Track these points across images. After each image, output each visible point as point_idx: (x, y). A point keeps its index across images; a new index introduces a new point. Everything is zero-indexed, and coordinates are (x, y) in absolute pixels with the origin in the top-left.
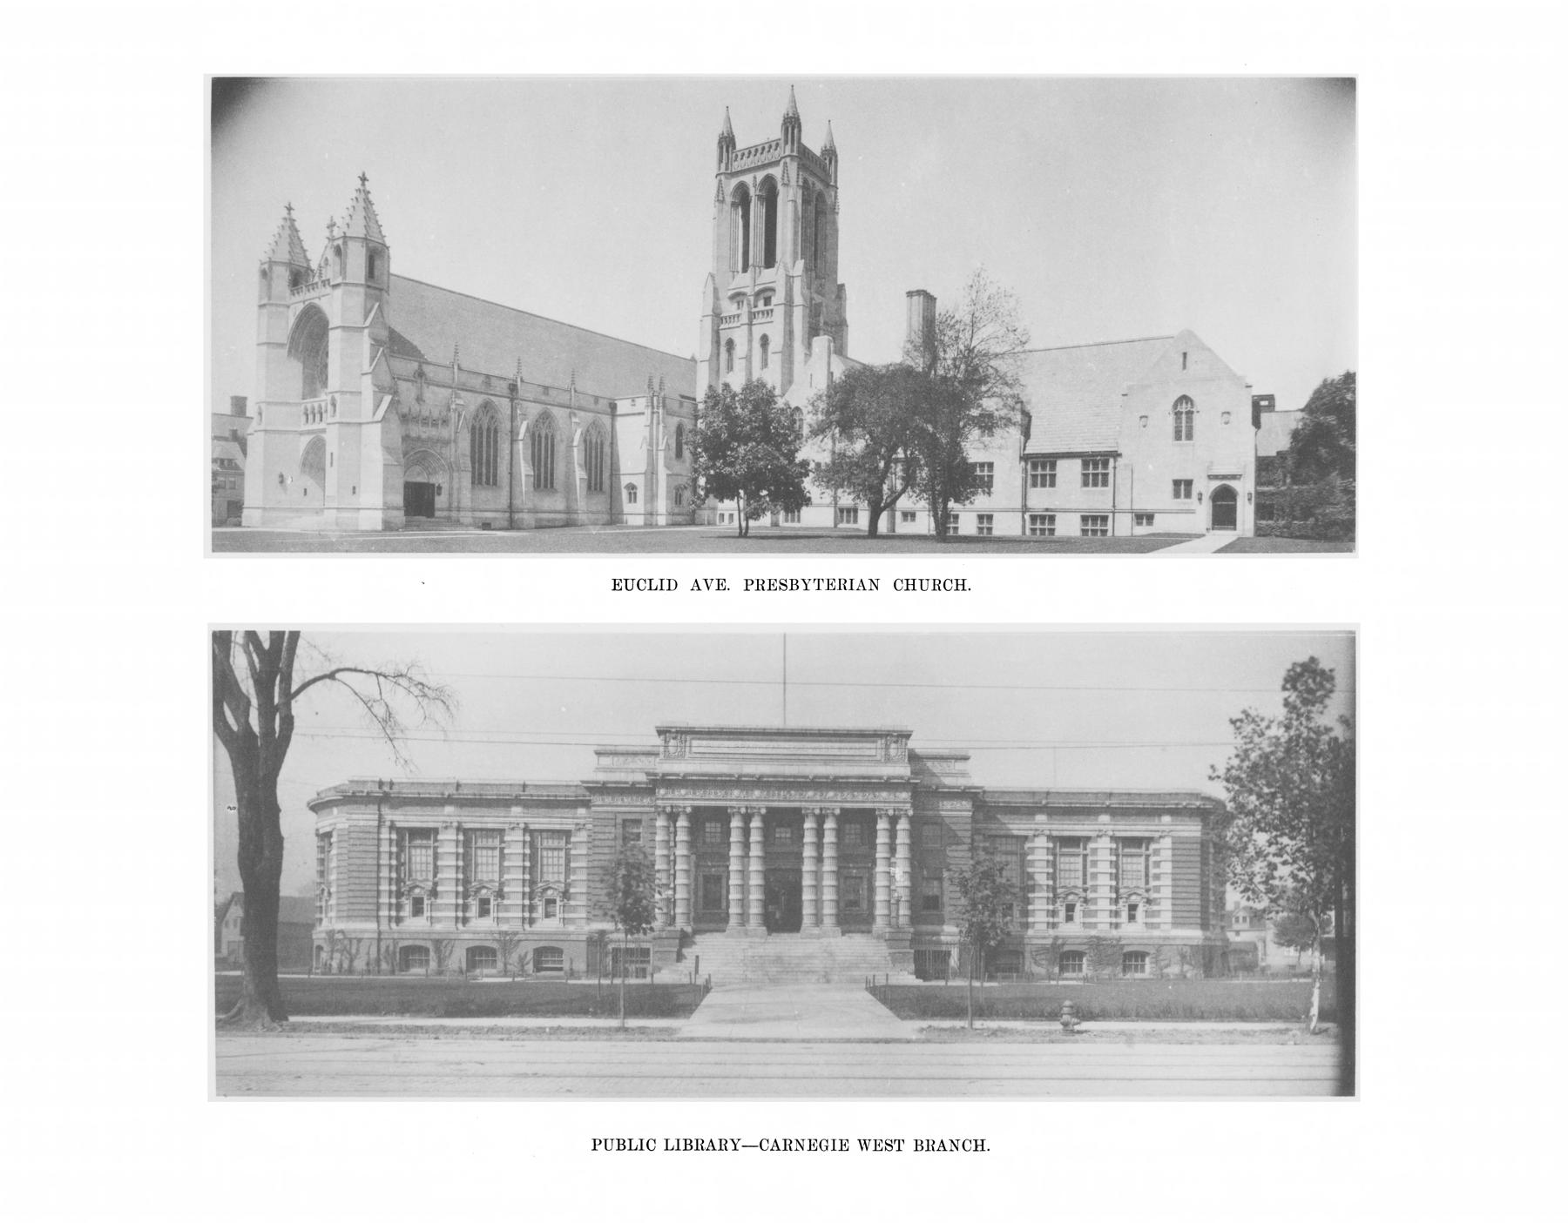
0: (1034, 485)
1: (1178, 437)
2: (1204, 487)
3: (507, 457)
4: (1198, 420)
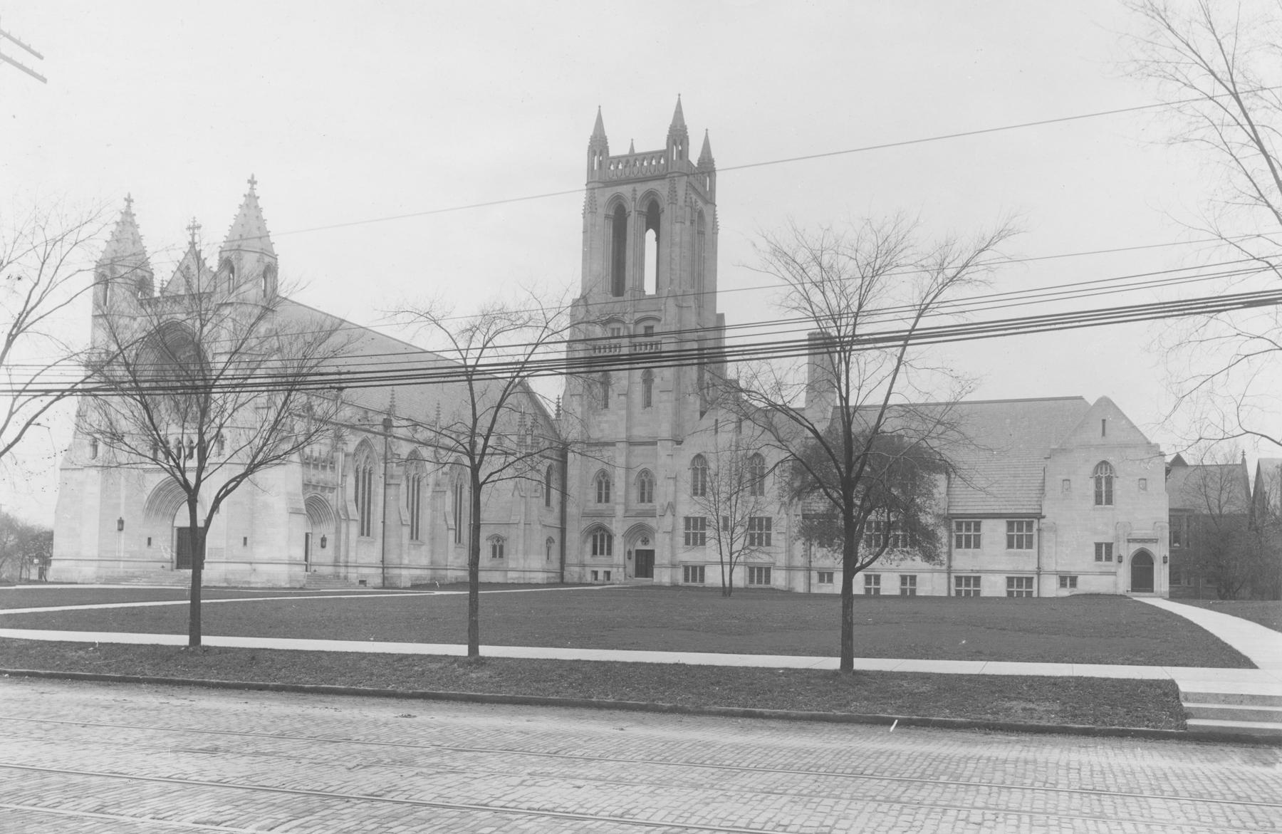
0: (959, 546)
1: (1098, 502)
2: (1128, 551)
3: (381, 504)
4: (1117, 486)
